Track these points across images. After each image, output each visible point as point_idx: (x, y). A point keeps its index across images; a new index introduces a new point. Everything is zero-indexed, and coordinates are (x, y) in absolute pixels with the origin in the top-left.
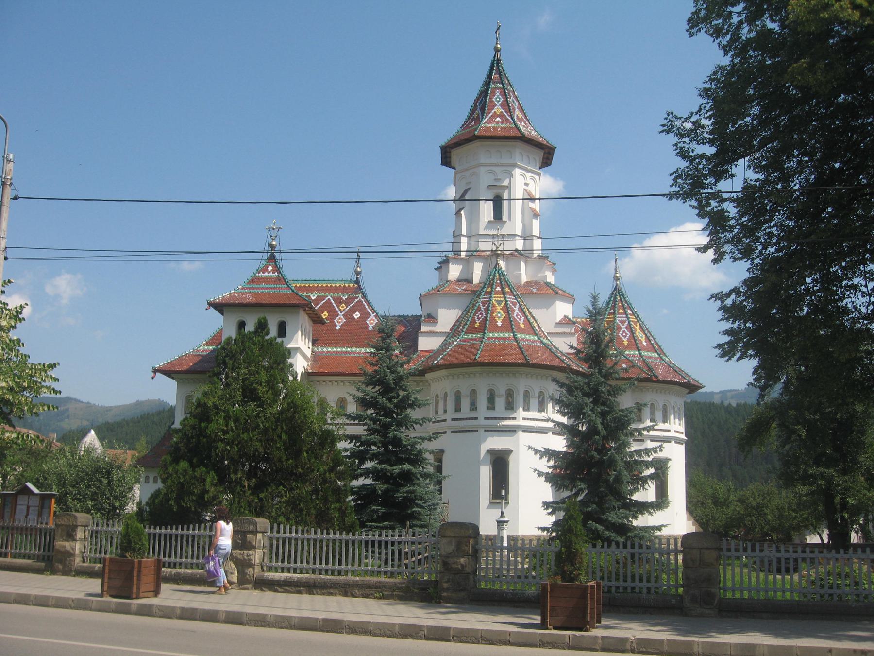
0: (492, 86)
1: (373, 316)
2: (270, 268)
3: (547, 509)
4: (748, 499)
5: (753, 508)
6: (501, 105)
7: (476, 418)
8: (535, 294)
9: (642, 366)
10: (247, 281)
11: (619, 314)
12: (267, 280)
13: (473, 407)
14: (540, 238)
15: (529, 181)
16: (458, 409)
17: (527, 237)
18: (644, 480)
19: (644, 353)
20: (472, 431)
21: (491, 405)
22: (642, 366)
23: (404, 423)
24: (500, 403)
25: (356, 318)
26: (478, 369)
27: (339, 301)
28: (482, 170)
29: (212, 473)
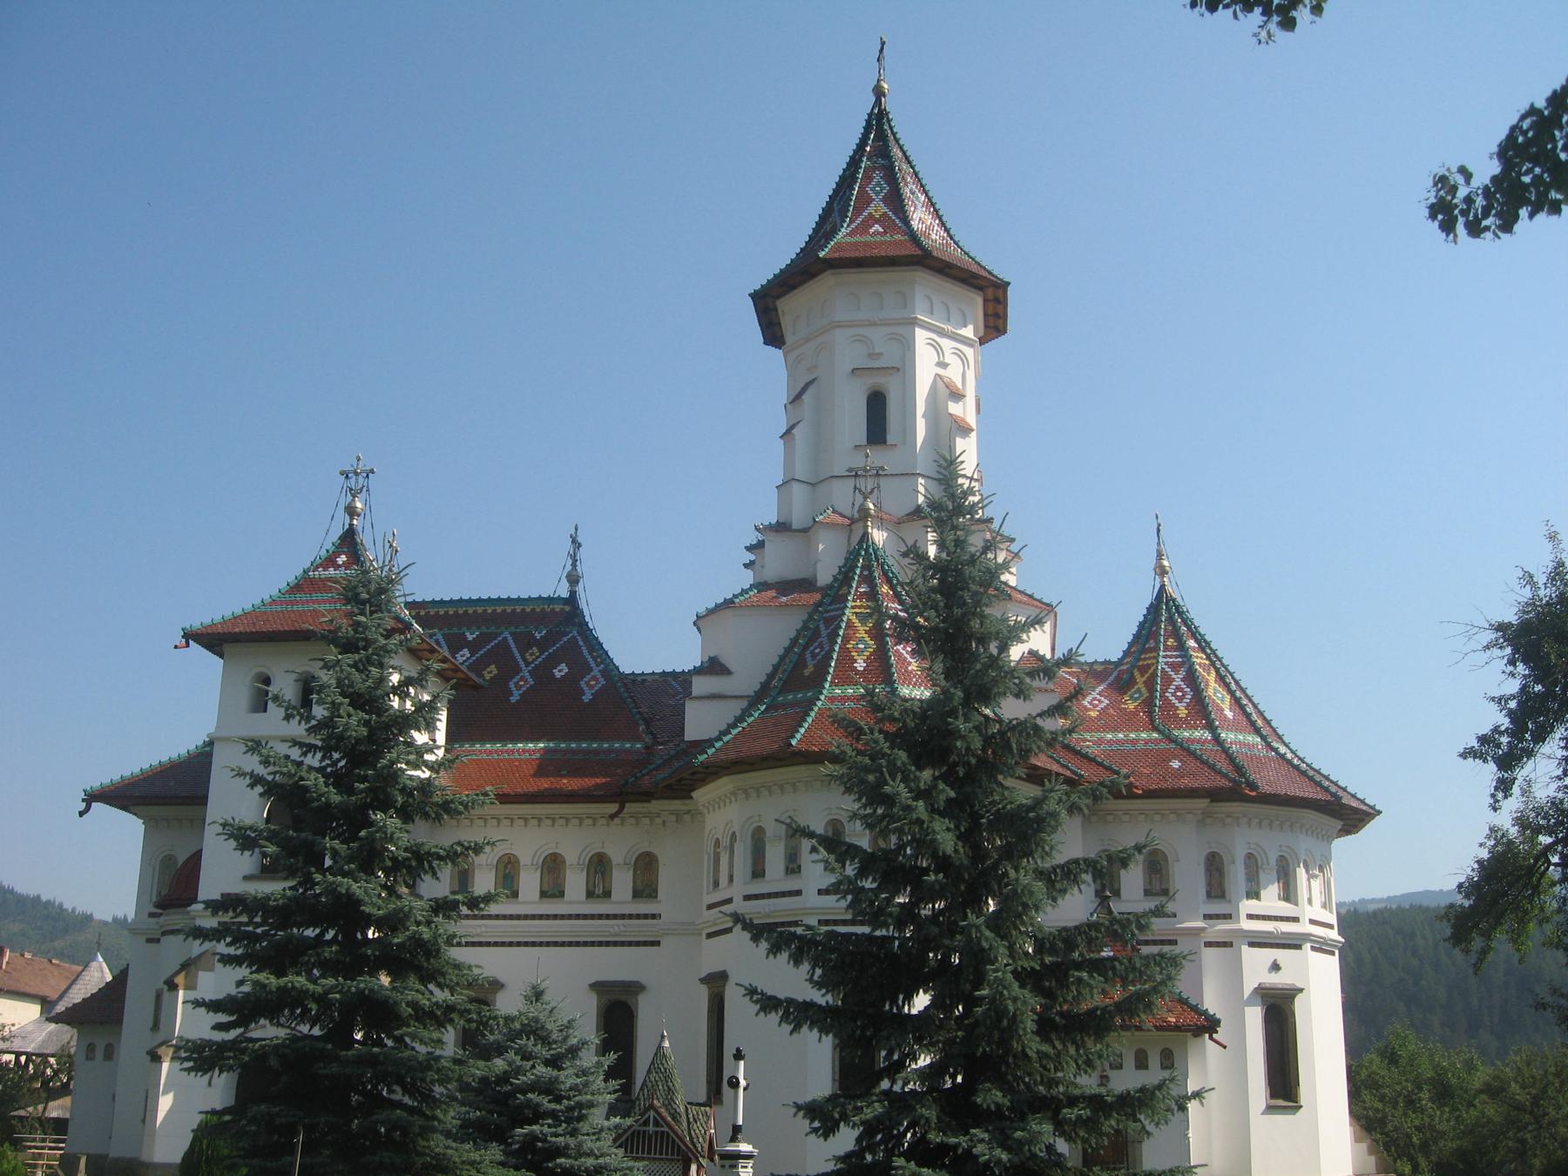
1: (596, 672)
2: (342, 559)
5: (1519, 1108)
6: (884, 200)
7: (798, 893)
9: (1223, 765)
15: (949, 358)
16: (758, 873)
19: (1228, 736)
22: (1223, 765)
25: (558, 675)
27: (526, 643)
28: (840, 336)
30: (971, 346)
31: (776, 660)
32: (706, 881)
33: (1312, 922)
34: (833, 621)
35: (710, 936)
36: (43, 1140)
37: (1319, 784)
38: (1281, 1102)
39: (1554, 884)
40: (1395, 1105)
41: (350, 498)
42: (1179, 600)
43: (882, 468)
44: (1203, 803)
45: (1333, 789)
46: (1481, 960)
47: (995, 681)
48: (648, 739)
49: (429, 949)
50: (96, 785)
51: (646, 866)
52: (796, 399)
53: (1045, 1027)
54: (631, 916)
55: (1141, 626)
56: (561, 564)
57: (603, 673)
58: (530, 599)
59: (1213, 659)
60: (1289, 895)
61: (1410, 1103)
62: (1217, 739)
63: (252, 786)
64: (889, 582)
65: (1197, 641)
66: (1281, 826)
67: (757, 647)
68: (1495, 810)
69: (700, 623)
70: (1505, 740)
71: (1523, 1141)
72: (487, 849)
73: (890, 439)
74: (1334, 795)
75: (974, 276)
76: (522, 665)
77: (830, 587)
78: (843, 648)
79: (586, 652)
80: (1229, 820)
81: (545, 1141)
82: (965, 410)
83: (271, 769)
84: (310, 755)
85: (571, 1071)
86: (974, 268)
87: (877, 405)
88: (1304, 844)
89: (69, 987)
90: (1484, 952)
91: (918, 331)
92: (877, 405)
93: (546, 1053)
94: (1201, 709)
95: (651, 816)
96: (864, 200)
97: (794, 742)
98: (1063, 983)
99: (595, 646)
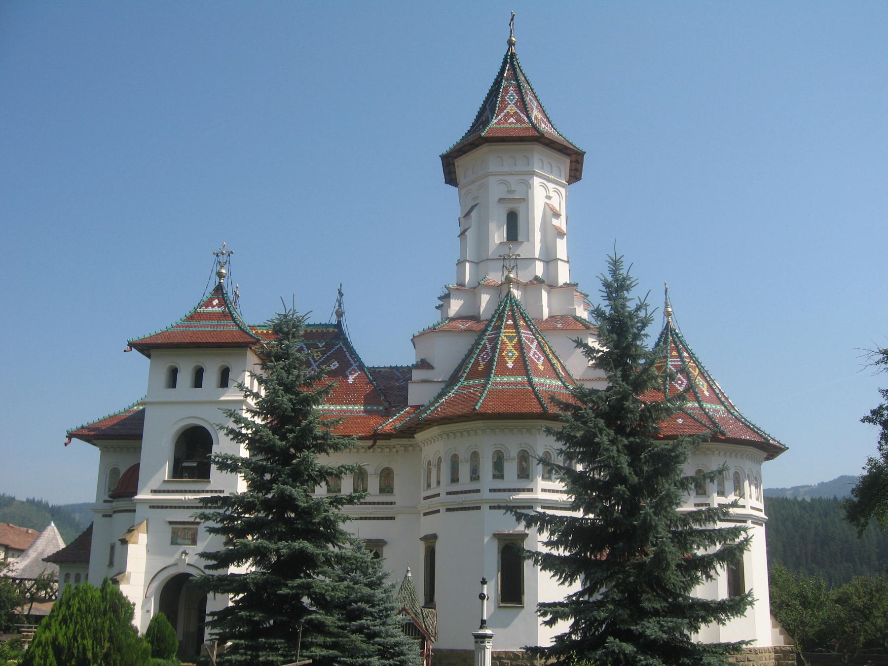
0: (504, 83)
1: (354, 366)
2: (216, 302)
3: (544, 614)
4: (850, 598)
6: (515, 104)
7: (478, 491)
8: (560, 329)
9: (705, 421)
10: (184, 318)
11: (672, 357)
13: (475, 476)
14: (568, 262)
15: (552, 194)
16: (455, 479)
17: (550, 260)
18: (705, 565)
19: (707, 406)
20: (473, 508)
21: (499, 472)
23: (302, 476)
24: (511, 469)
26: (480, 424)
28: (492, 180)
29: (602, 597)
33: (752, 508)
35: (425, 514)
36: (29, 627)
37: (757, 433)
41: (219, 267)
43: (519, 255)
48: (386, 404)
49: (329, 523)
50: (74, 428)
51: (387, 475)
52: (468, 214)
54: (378, 503)
56: (332, 305)
59: (698, 364)
62: (701, 408)
63: (227, 435)
64: (524, 319)
66: (719, 454)
67: (447, 354)
71: (854, 628)
72: (67, 440)
73: (520, 239)
75: (566, 148)
76: (313, 362)
79: (348, 355)
80: (708, 452)
81: (368, 628)
82: (561, 223)
84: (256, 417)
86: (566, 144)
88: (747, 465)
93: (366, 581)
96: (504, 105)
97: (477, 408)
99: (352, 352)
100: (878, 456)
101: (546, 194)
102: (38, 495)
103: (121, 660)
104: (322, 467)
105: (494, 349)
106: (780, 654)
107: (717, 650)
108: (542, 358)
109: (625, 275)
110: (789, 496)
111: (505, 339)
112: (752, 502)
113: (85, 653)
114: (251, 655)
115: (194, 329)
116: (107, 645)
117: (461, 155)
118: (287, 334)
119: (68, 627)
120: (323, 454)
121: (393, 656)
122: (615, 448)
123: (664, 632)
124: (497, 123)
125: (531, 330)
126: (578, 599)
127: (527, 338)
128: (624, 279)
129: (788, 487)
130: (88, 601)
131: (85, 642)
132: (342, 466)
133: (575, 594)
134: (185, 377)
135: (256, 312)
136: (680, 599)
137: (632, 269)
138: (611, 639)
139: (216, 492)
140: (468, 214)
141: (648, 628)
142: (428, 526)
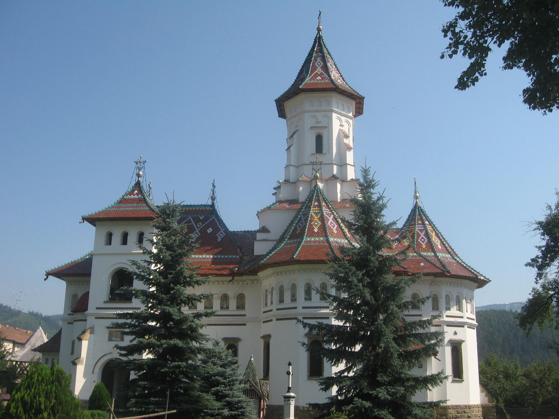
0: (314, 54)
1: (222, 231)
5: (536, 381)
7: (296, 308)
9: (438, 265)
11: (418, 224)
12: (133, 201)
14: (353, 166)
16: (281, 301)
17: (343, 165)
19: (440, 255)
21: (308, 297)
25: (209, 232)
26: (296, 266)
27: (197, 220)
28: (307, 115)
30: (351, 119)
31: (286, 228)
32: (263, 303)
33: (468, 318)
34: (306, 215)
35: (264, 322)
37: (470, 271)
38: (457, 379)
39: (554, 307)
40: (491, 380)
41: (138, 171)
42: (422, 208)
44: (431, 278)
45: (475, 273)
46: (528, 333)
47: (382, 243)
48: (241, 254)
49: (193, 330)
50: (50, 270)
51: (241, 298)
52: (292, 137)
53: (400, 355)
54: (236, 315)
55: (409, 216)
56: (209, 193)
57: (224, 231)
58: (198, 205)
59: (434, 227)
60: (460, 309)
61: (496, 378)
62: (436, 256)
64: (325, 201)
65: (428, 222)
67: (279, 223)
68: (537, 283)
69: (259, 215)
70: (540, 260)
71: (536, 392)
73: (324, 151)
74: (476, 275)
75: (352, 95)
76: (196, 228)
77: (304, 203)
78: (310, 224)
79: (218, 224)
80: (440, 283)
81: (222, 392)
82: (349, 142)
83: (140, 270)
85: (229, 369)
86: (353, 92)
87: (319, 139)
88: (465, 291)
89: (30, 338)
90: (530, 329)
91: (333, 114)
92: (319, 139)
93: (221, 363)
94: (431, 246)
95: (243, 281)
96: (315, 68)
97: (295, 257)
98: (405, 342)
100: (538, 287)
101: (341, 123)
102: (36, 309)
103: (62, 410)
104: (189, 295)
105: (306, 220)
106: (485, 409)
107: (425, 406)
108: (336, 226)
109: (371, 179)
110: (507, 309)
111: (313, 214)
112: (468, 313)
113: (40, 406)
114: (145, 408)
115: (122, 209)
116: (53, 401)
117: (287, 100)
118: (169, 215)
119: (31, 390)
120: (191, 287)
121: (237, 409)
122: (361, 284)
123: (390, 395)
124: (310, 80)
125: (329, 208)
126: (341, 375)
127: (326, 213)
128: (371, 181)
129: (507, 303)
130: (43, 375)
131: (41, 399)
132: (202, 295)
133: (339, 372)
134: (117, 239)
135: (157, 199)
136: (403, 375)
137: (376, 175)
138: (356, 399)
139: (136, 308)
140: (292, 137)
141: (380, 392)
142: (266, 329)
